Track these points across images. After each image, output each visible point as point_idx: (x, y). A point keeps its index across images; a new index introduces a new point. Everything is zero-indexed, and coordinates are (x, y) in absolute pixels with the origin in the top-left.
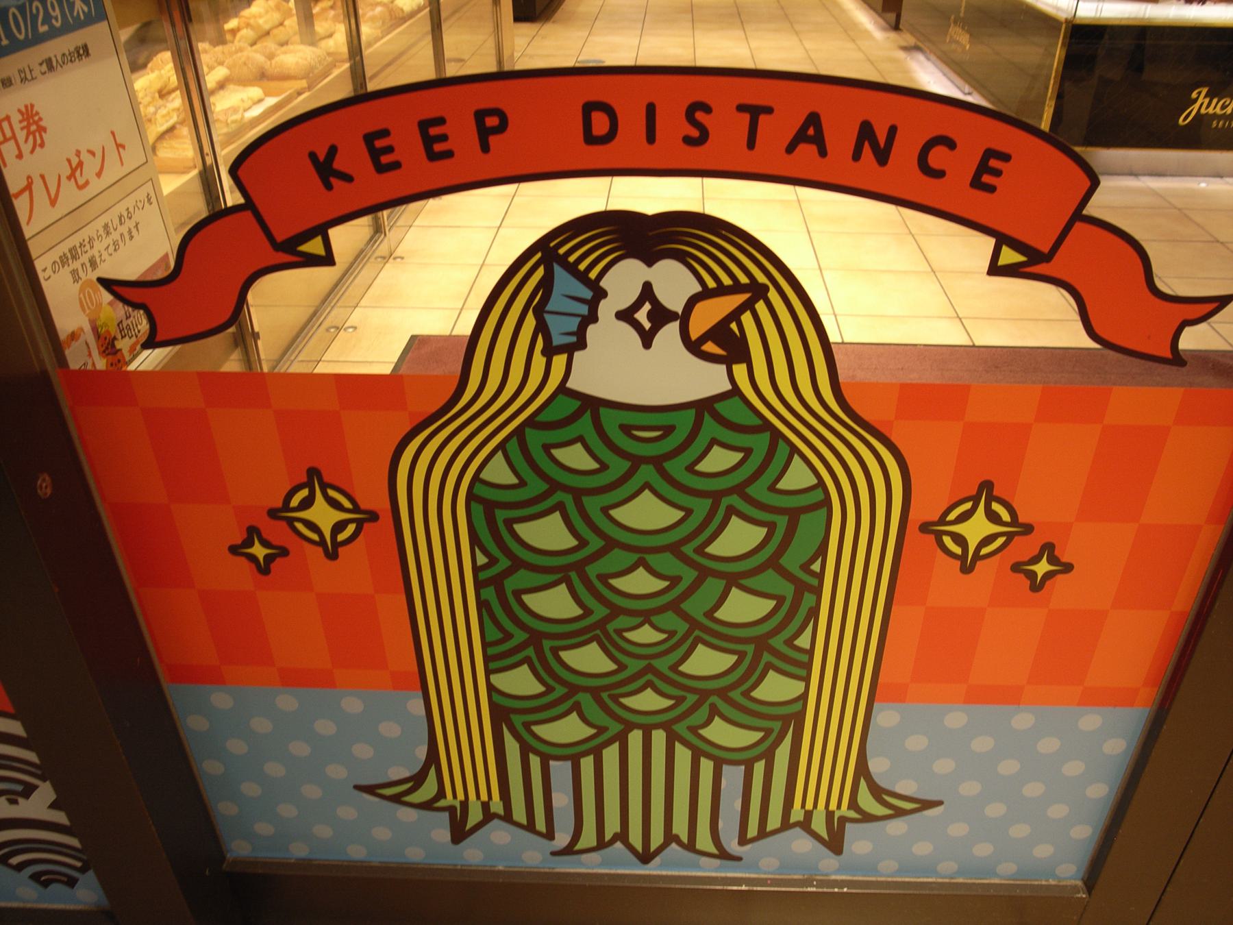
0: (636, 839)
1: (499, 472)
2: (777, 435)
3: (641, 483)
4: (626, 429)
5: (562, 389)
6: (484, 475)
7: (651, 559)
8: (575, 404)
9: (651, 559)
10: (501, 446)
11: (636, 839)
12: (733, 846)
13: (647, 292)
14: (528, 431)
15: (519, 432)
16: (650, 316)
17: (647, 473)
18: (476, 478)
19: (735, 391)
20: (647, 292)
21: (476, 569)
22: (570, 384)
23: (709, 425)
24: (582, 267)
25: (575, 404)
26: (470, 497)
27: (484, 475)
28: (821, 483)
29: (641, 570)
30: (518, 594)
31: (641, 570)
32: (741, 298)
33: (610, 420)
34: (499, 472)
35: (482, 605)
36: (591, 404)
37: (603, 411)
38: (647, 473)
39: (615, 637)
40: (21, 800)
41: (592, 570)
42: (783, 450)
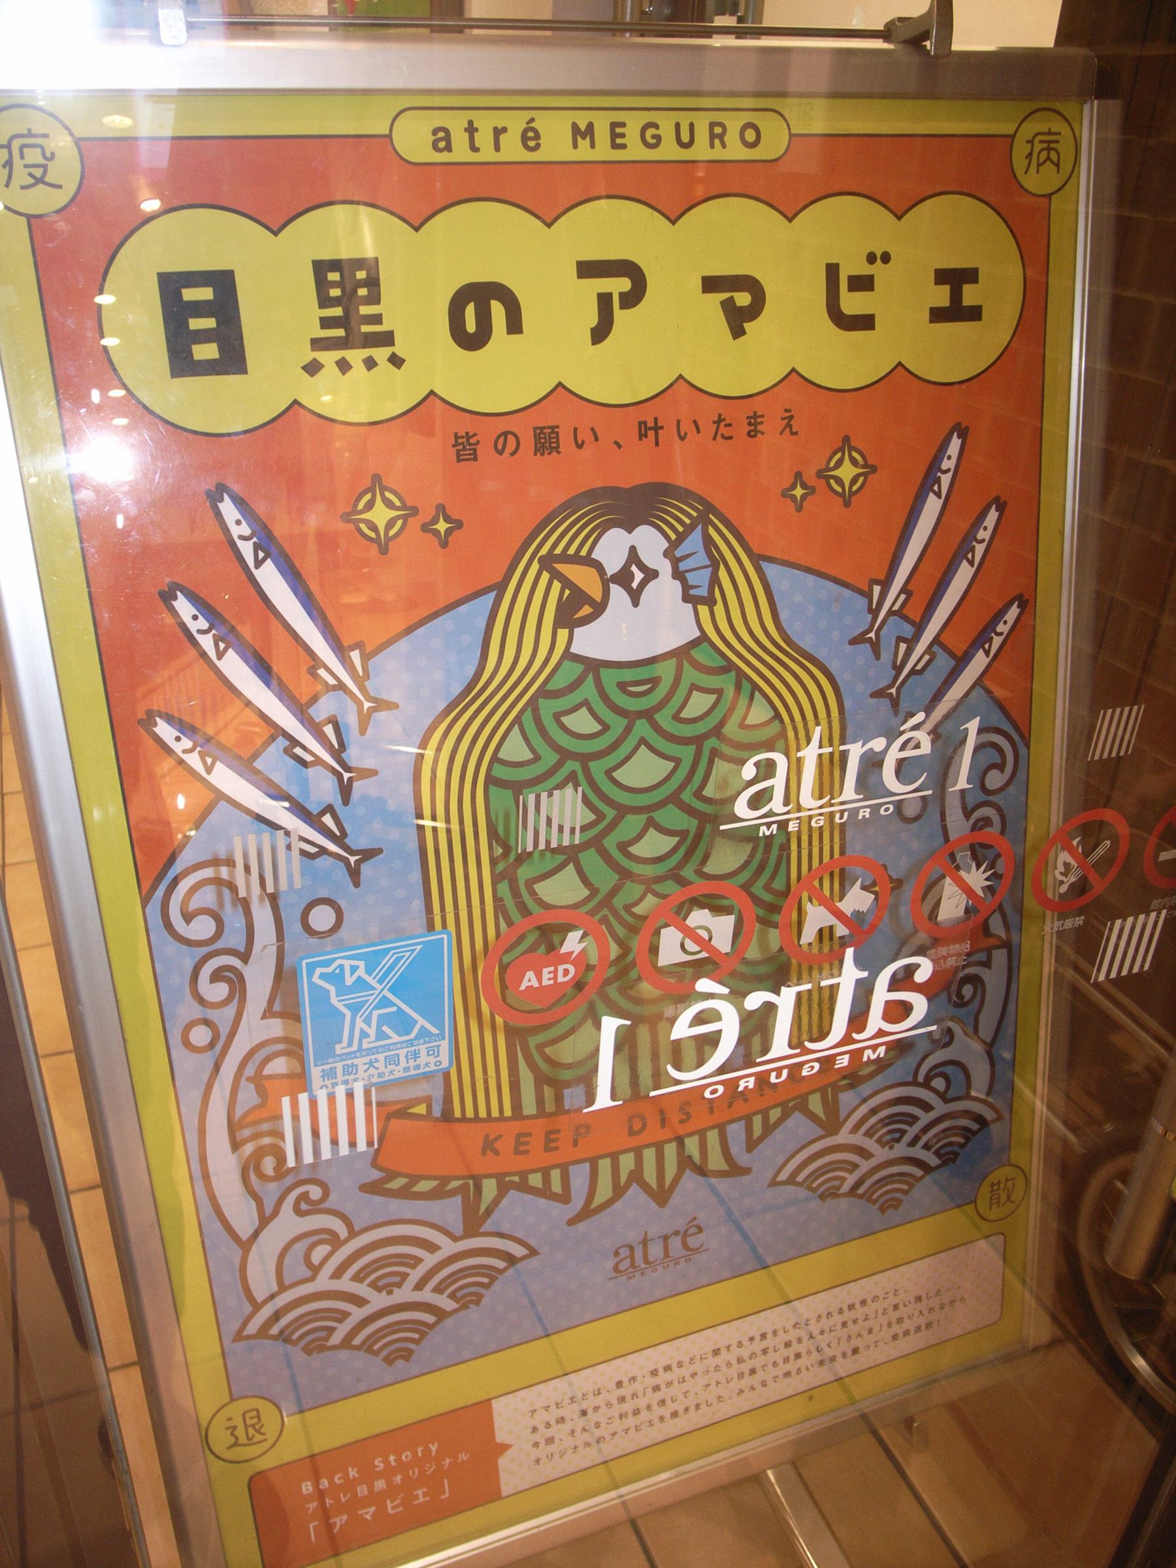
0: (650, 1176)
1: (516, 749)
2: (741, 674)
3: (540, 752)
4: (622, 686)
5: (568, 655)
6: (502, 755)
7: (658, 816)
8: (579, 668)
9: (658, 816)
10: (518, 720)
11: (650, 1176)
12: (743, 1159)
13: (633, 556)
14: (541, 701)
15: (533, 702)
16: (632, 576)
17: (642, 728)
18: (495, 758)
19: (703, 638)
20: (633, 556)
21: (493, 862)
22: (573, 650)
23: (688, 670)
24: (680, 529)
25: (579, 668)
26: (490, 780)
27: (502, 755)
28: (777, 715)
29: (652, 831)
30: (530, 884)
31: (652, 831)
32: (561, 567)
33: (610, 678)
34: (516, 749)
35: (497, 899)
36: (593, 666)
37: (604, 673)
38: (642, 728)
39: (623, 913)
40: (395, 1290)
41: (610, 843)
42: (746, 686)
